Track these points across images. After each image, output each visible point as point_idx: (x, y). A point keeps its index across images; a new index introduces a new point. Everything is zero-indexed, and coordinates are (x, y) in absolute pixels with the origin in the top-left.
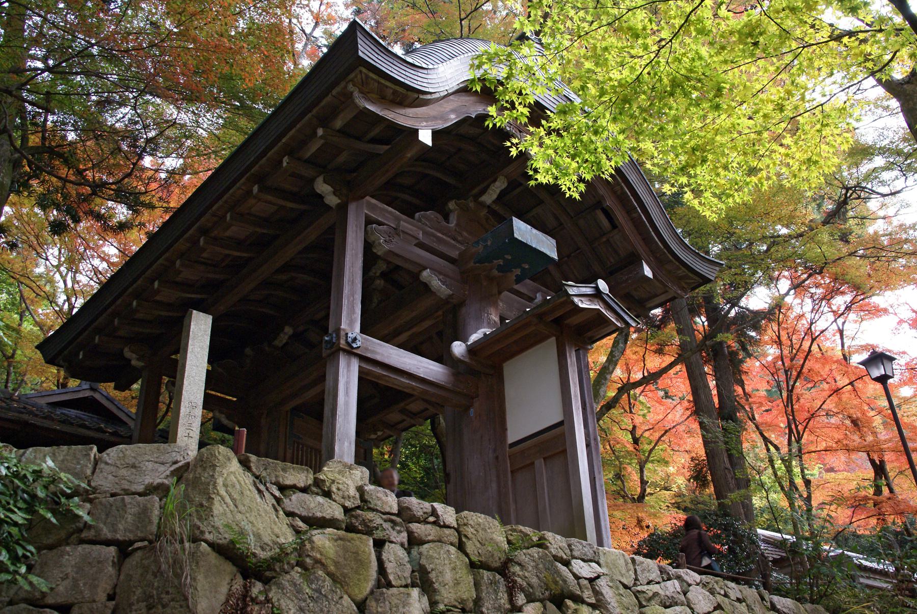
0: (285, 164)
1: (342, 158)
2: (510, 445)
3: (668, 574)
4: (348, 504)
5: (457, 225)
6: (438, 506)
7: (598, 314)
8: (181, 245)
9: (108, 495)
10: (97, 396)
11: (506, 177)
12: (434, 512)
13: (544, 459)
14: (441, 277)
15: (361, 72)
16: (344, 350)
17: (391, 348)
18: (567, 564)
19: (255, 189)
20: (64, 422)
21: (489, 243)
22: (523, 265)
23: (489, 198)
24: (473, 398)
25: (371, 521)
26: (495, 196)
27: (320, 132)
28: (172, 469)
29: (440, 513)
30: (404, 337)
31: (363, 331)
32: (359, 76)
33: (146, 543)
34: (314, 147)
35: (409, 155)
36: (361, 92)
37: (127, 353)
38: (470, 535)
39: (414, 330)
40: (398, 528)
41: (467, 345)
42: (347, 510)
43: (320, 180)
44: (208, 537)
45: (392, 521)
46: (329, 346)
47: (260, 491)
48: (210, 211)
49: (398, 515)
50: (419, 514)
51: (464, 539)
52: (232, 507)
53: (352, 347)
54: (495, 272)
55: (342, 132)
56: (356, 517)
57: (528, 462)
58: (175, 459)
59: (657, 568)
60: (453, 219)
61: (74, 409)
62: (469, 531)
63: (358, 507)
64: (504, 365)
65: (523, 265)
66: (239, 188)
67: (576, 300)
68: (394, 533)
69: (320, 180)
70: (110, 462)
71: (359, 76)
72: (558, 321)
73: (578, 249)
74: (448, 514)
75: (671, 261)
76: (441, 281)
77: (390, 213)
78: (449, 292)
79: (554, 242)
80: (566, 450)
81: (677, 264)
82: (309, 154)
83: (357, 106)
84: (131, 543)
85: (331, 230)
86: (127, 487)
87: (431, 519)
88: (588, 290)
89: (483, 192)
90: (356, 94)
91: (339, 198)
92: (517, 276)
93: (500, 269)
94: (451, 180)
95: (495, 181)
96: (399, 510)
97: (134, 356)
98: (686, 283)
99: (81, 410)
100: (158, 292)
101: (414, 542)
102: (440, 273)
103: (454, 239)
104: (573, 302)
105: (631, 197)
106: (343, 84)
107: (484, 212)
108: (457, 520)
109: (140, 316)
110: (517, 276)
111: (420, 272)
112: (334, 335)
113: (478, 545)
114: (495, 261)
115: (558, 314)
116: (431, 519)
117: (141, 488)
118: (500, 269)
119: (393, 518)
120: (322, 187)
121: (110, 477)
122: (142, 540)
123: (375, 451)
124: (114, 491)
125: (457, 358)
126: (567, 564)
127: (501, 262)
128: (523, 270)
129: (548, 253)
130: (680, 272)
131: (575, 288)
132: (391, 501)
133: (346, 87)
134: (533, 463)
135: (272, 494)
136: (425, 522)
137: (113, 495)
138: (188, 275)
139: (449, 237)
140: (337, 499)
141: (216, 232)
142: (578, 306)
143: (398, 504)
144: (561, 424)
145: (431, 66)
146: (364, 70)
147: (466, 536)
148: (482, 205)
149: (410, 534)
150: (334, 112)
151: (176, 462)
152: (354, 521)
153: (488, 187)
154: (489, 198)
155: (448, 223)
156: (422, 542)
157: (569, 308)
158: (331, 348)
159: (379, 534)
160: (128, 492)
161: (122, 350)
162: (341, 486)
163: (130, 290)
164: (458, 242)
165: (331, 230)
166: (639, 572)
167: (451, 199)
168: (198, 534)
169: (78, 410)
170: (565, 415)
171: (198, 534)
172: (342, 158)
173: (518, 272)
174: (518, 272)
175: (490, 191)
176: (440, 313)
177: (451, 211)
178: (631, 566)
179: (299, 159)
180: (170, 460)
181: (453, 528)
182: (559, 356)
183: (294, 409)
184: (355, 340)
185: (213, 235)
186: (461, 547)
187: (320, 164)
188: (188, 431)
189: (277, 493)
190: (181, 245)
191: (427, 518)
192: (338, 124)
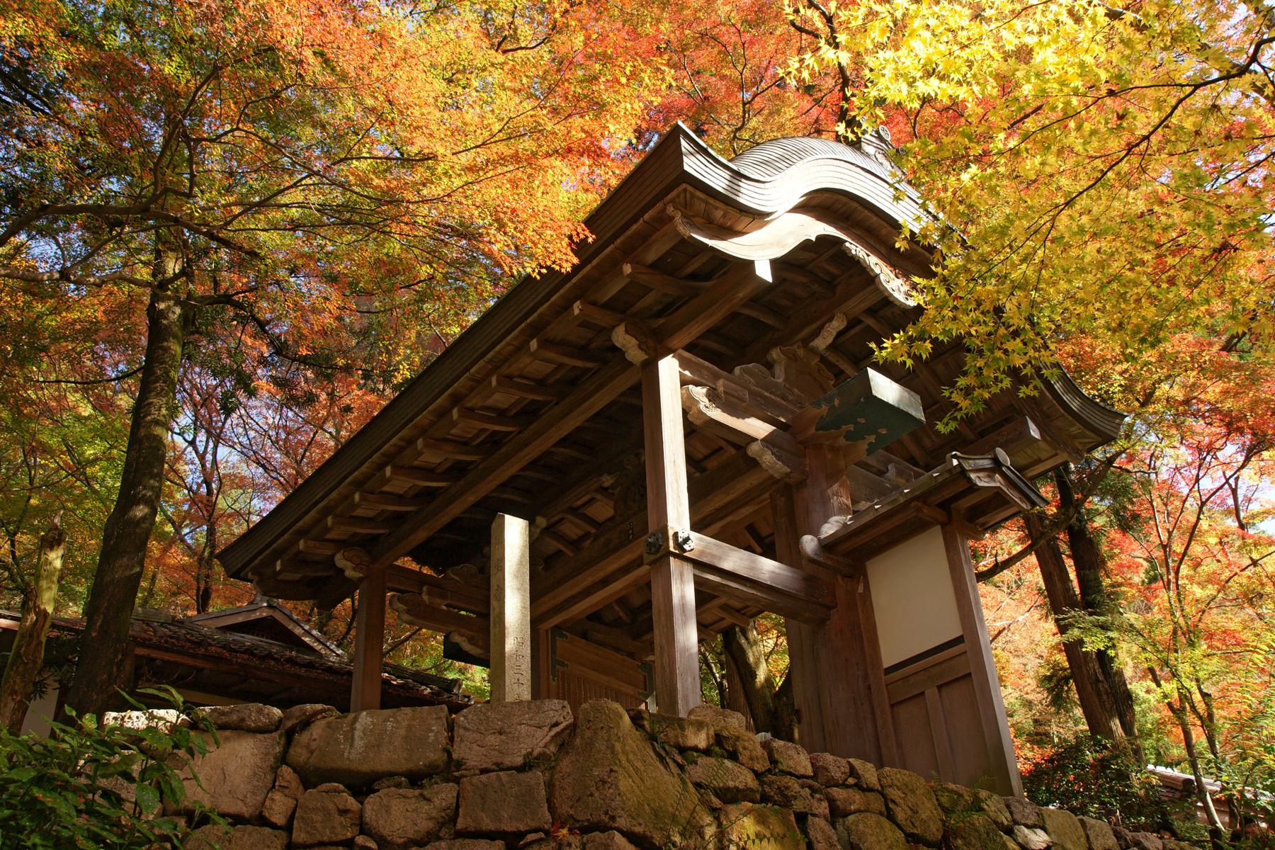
0: (576, 312)
1: (648, 300)
2: (886, 669)
3: (1126, 840)
4: (758, 767)
5: (785, 380)
6: (856, 763)
7: (997, 493)
8: (423, 418)
9: (478, 772)
10: (278, 616)
11: (845, 314)
12: (853, 772)
13: (940, 687)
14: (775, 450)
15: (685, 190)
16: (675, 555)
17: (730, 549)
18: (1009, 832)
19: (534, 344)
20: (224, 647)
21: (837, 402)
22: (880, 431)
23: (822, 343)
24: (830, 608)
25: (787, 788)
26: (830, 340)
27: (628, 269)
28: (553, 733)
29: (860, 772)
30: (717, 526)
31: (696, 526)
32: (682, 196)
33: (542, 835)
34: (614, 288)
35: (741, 295)
36: (684, 216)
37: (340, 561)
38: (898, 800)
39: (729, 519)
40: (818, 796)
41: (819, 540)
42: (758, 775)
43: (620, 331)
44: (622, 822)
45: (810, 787)
46: (653, 549)
47: (662, 759)
48: (467, 374)
49: (814, 777)
50: (838, 775)
51: (891, 805)
52: (638, 781)
53: (685, 551)
54: (842, 441)
55: (656, 266)
56: (770, 784)
57: (916, 692)
58: (555, 720)
59: (1111, 832)
60: (779, 371)
61: (248, 634)
62: (894, 793)
63: (769, 771)
64: (868, 564)
65: (880, 431)
66: (509, 344)
67: (973, 476)
68: (816, 804)
69: (620, 331)
70: (468, 726)
71: (682, 196)
72: (945, 505)
73: (936, 403)
74: (869, 773)
75: (1063, 415)
76: (776, 456)
77: (707, 368)
78: (787, 470)
79: (875, 393)
80: (969, 674)
81: (1070, 418)
82: (606, 299)
83: (678, 233)
84: (522, 835)
85: (636, 390)
86: (499, 760)
87: (851, 781)
88: (986, 463)
89: (816, 334)
90: (678, 218)
91: (647, 353)
92: (870, 444)
93: (849, 436)
94: (769, 321)
95: (831, 319)
96: (814, 772)
97: (349, 564)
98: (1081, 443)
99: (258, 635)
100: (389, 480)
101: (837, 813)
102: (774, 446)
103: (784, 398)
104: (969, 479)
105: (528, 321)
106: (659, 206)
107: (816, 360)
108: (879, 780)
109: (360, 512)
110: (870, 444)
111: (748, 444)
112: (660, 535)
113: (909, 812)
114: (844, 427)
115: (947, 494)
116: (851, 781)
117: (519, 760)
118: (849, 436)
119: (810, 781)
120: (621, 337)
121: (475, 747)
122: (536, 831)
123: (74, 610)
124: (484, 766)
125: (806, 553)
126: (1009, 832)
127: (851, 427)
128: (879, 435)
129: (914, 413)
130: (1074, 429)
131: (971, 462)
132: (801, 761)
133: (665, 209)
134: (923, 693)
135: (675, 762)
136: (845, 786)
137: (484, 771)
138: (431, 458)
139: (778, 396)
140: (744, 761)
141: (474, 401)
142: (975, 484)
143: (812, 764)
144: (958, 640)
145: (768, 179)
146: (690, 188)
147: (893, 801)
148: (814, 351)
149: (832, 802)
150: (644, 239)
151: (556, 724)
152: (767, 789)
153: (821, 328)
154: (822, 343)
155: (774, 377)
156: (846, 814)
157: (962, 486)
158: (657, 552)
159: (798, 806)
160: (500, 767)
161: (333, 556)
162: (746, 744)
163: (350, 479)
164: (789, 401)
165: (636, 390)
166: (1092, 838)
167: (774, 345)
168: (607, 820)
169: (253, 634)
170: (964, 628)
171: (607, 820)
172: (648, 300)
173: (872, 439)
174: (872, 439)
175: (824, 333)
176: (767, 495)
177: (774, 361)
178: (1080, 829)
179: (594, 304)
180: (548, 721)
181: (877, 790)
182: (946, 544)
183: (556, 626)
184: (687, 540)
185: (469, 405)
186: (891, 817)
187: (620, 307)
188: (517, 676)
189: (679, 759)
190: (423, 418)
191: (846, 780)
192: (652, 256)
